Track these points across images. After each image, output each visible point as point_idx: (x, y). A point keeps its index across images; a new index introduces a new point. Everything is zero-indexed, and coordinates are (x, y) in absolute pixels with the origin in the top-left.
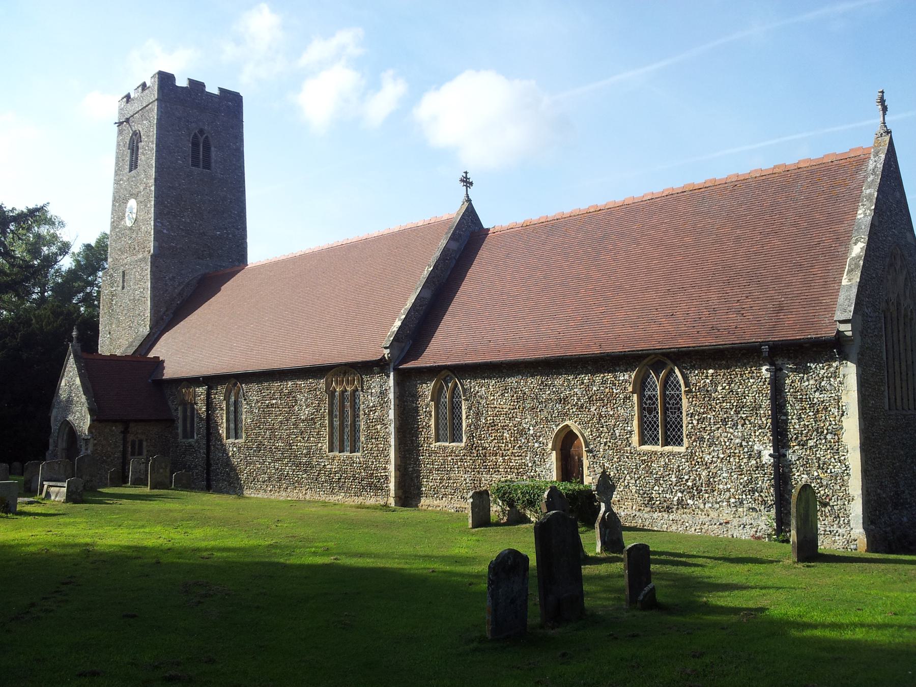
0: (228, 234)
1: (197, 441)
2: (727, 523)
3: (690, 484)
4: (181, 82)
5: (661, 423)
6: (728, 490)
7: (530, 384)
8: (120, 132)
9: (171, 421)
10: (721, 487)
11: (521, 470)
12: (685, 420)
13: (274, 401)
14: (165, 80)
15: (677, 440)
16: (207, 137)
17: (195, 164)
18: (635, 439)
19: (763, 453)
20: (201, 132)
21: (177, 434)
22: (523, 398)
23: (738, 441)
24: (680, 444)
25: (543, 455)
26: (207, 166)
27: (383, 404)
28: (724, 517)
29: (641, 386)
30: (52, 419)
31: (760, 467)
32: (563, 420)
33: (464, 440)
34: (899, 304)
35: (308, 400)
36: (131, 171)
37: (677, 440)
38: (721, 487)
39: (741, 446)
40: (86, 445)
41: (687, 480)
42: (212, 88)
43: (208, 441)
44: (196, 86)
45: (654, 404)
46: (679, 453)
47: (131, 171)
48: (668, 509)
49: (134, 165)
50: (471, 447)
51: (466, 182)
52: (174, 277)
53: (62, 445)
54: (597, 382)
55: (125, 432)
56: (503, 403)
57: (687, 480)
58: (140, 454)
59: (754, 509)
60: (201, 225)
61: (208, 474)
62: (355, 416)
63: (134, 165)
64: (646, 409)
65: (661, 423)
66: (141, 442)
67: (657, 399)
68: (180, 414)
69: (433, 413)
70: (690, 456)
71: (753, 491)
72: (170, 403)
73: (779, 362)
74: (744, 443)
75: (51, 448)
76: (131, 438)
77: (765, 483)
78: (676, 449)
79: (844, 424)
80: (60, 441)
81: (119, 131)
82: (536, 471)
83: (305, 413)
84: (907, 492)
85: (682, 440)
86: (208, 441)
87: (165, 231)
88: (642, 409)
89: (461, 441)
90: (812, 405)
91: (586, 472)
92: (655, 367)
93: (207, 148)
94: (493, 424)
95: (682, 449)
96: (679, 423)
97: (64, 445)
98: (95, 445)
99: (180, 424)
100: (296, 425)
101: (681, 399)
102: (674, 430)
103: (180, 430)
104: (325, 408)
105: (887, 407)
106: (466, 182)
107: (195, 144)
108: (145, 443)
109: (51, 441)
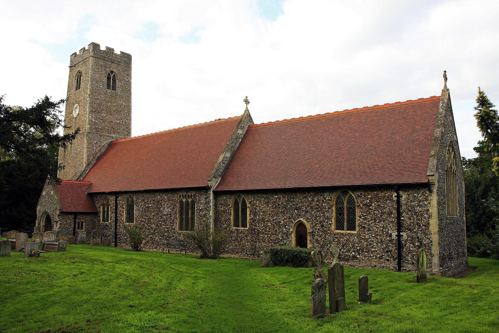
0: (123, 122)
1: (110, 223)
2: (375, 266)
3: (358, 248)
4: (103, 48)
5: (346, 219)
6: (376, 251)
7: (282, 200)
8: (71, 71)
9: (96, 214)
10: (373, 249)
11: (277, 241)
12: (357, 218)
13: (150, 205)
14: (95, 46)
15: (353, 228)
16: (114, 75)
17: (108, 87)
18: (333, 227)
19: (393, 234)
20: (112, 72)
21: (100, 220)
22: (277, 207)
23: (381, 228)
24: (354, 230)
25: (288, 234)
26: (114, 88)
27: (207, 209)
28: (373, 264)
29: (339, 202)
30: (38, 211)
31: (391, 241)
32: (298, 218)
33: (248, 226)
34: (451, 168)
35: (122, 201)
36: (76, 90)
37: (353, 228)
38: (373, 249)
39: (383, 231)
40: (56, 224)
41: (357, 247)
42: (117, 52)
43: (116, 223)
44: (110, 51)
45: (342, 211)
46: (354, 234)
47: (76, 90)
48: (348, 260)
49: (78, 87)
50: (251, 229)
51: (247, 102)
52: (97, 143)
53: (43, 224)
54: (316, 199)
55: (75, 219)
56: (269, 209)
57: (357, 247)
58: (82, 229)
59: (388, 260)
60: (110, 117)
61: (116, 239)
62: (193, 213)
63: (78, 87)
64: (340, 213)
65: (346, 219)
66: (82, 223)
67: (344, 209)
68: (101, 210)
69: (232, 213)
70: (359, 235)
71: (388, 252)
72: (96, 204)
73: (401, 193)
74: (384, 230)
75: (37, 225)
76: (77, 221)
77: (393, 248)
78: (352, 232)
79: (430, 222)
80: (41, 222)
81: (70, 70)
82: (284, 242)
83: (166, 211)
84: (453, 252)
85: (355, 228)
86: (116, 223)
87: (93, 120)
88: (337, 214)
89: (247, 227)
90: (416, 213)
91: (308, 242)
92: (345, 196)
93: (114, 81)
94: (263, 220)
95: (355, 232)
96: (354, 220)
97: (44, 224)
98: (60, 224)
99: (101, 215)
100: (161, 217)
101: (355, 209)
102: (351, 223)
103: (101, 218)
104: (177, 209)
105: (446, 214)
106: (247, 102)
107: (109, 78)
108: (84, 224)
109: (37, 222)
